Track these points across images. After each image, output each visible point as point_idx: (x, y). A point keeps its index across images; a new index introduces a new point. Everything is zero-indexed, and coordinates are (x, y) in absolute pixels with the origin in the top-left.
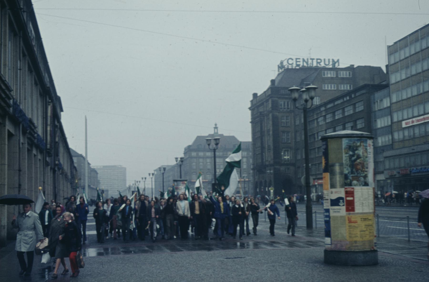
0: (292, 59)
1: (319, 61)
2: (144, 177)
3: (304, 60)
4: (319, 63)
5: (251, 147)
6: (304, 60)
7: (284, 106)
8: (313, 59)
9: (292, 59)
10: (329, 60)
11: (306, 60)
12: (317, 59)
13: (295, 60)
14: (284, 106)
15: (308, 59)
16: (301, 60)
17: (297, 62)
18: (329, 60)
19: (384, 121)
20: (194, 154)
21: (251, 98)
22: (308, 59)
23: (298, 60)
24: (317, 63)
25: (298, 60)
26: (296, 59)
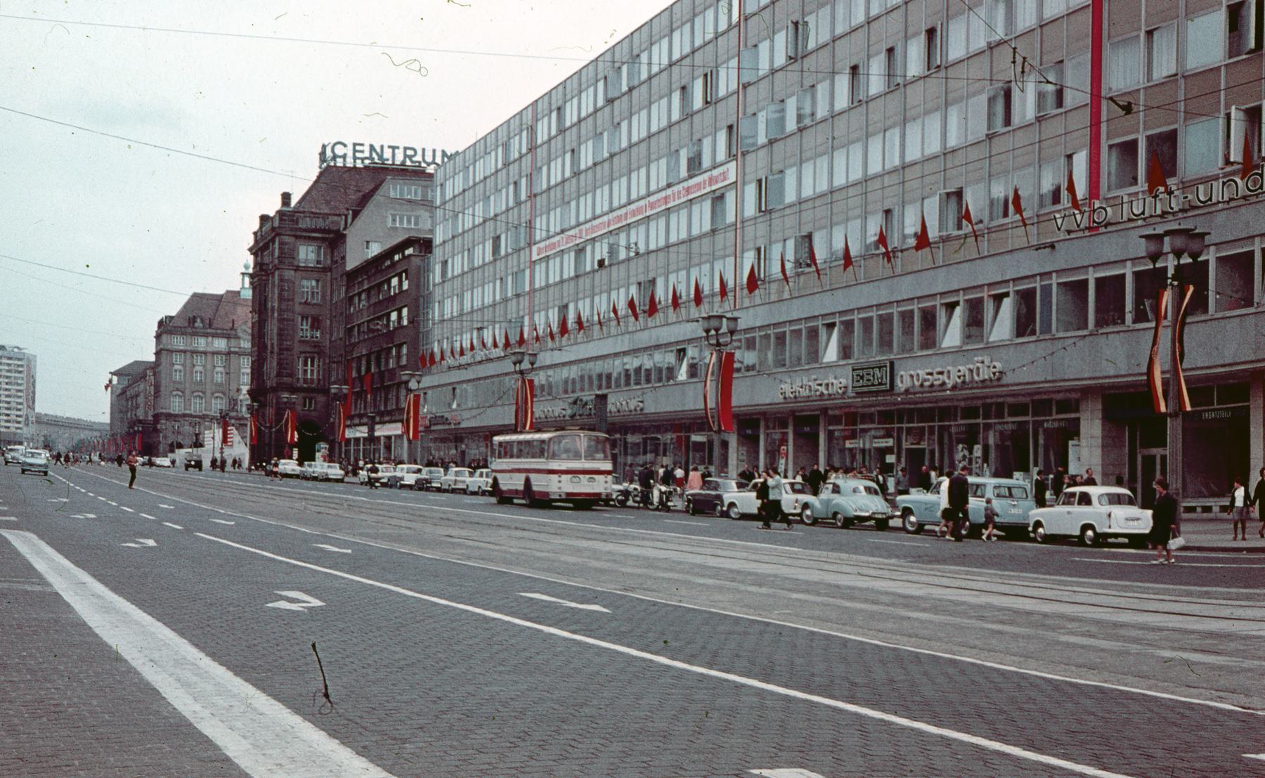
0: (345, 146)
1: (409, 152)
2: (218, 472)
3: (372, 148)
4: (410, 157)
5: (244, 318)
6: (372, 148)
7: (357, 451)
8: (394, 148)
9: (345, 146)
10: (434, 151)
11: (379, 150)
12: (406, 149)
13: (350, 147)
14: (357, 451)
15: (382, 147)
16: (367, 149)
17: (355, 151)
18: (434, 151)
19: (611, 190)
20: (178, 342)
21: (256, 226)
22: (382, 147)
23: (358, 148)
24: (406, 156)
25: (358, 148)
26: (355, 145)
